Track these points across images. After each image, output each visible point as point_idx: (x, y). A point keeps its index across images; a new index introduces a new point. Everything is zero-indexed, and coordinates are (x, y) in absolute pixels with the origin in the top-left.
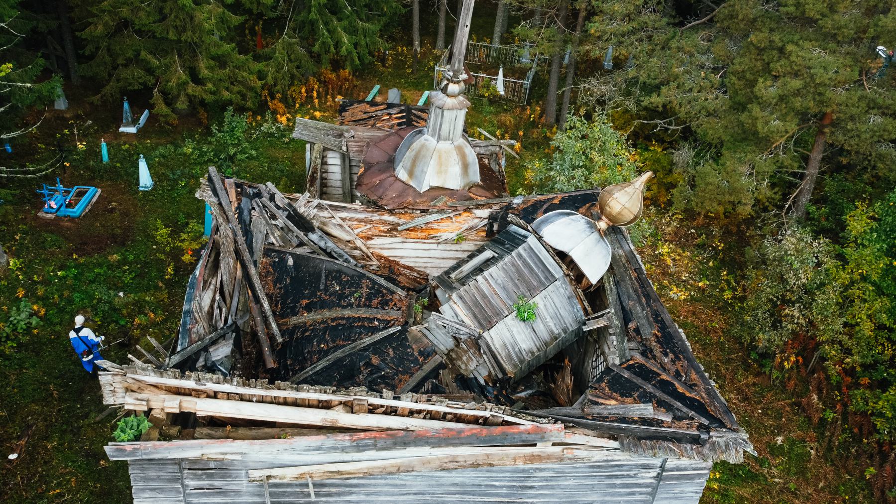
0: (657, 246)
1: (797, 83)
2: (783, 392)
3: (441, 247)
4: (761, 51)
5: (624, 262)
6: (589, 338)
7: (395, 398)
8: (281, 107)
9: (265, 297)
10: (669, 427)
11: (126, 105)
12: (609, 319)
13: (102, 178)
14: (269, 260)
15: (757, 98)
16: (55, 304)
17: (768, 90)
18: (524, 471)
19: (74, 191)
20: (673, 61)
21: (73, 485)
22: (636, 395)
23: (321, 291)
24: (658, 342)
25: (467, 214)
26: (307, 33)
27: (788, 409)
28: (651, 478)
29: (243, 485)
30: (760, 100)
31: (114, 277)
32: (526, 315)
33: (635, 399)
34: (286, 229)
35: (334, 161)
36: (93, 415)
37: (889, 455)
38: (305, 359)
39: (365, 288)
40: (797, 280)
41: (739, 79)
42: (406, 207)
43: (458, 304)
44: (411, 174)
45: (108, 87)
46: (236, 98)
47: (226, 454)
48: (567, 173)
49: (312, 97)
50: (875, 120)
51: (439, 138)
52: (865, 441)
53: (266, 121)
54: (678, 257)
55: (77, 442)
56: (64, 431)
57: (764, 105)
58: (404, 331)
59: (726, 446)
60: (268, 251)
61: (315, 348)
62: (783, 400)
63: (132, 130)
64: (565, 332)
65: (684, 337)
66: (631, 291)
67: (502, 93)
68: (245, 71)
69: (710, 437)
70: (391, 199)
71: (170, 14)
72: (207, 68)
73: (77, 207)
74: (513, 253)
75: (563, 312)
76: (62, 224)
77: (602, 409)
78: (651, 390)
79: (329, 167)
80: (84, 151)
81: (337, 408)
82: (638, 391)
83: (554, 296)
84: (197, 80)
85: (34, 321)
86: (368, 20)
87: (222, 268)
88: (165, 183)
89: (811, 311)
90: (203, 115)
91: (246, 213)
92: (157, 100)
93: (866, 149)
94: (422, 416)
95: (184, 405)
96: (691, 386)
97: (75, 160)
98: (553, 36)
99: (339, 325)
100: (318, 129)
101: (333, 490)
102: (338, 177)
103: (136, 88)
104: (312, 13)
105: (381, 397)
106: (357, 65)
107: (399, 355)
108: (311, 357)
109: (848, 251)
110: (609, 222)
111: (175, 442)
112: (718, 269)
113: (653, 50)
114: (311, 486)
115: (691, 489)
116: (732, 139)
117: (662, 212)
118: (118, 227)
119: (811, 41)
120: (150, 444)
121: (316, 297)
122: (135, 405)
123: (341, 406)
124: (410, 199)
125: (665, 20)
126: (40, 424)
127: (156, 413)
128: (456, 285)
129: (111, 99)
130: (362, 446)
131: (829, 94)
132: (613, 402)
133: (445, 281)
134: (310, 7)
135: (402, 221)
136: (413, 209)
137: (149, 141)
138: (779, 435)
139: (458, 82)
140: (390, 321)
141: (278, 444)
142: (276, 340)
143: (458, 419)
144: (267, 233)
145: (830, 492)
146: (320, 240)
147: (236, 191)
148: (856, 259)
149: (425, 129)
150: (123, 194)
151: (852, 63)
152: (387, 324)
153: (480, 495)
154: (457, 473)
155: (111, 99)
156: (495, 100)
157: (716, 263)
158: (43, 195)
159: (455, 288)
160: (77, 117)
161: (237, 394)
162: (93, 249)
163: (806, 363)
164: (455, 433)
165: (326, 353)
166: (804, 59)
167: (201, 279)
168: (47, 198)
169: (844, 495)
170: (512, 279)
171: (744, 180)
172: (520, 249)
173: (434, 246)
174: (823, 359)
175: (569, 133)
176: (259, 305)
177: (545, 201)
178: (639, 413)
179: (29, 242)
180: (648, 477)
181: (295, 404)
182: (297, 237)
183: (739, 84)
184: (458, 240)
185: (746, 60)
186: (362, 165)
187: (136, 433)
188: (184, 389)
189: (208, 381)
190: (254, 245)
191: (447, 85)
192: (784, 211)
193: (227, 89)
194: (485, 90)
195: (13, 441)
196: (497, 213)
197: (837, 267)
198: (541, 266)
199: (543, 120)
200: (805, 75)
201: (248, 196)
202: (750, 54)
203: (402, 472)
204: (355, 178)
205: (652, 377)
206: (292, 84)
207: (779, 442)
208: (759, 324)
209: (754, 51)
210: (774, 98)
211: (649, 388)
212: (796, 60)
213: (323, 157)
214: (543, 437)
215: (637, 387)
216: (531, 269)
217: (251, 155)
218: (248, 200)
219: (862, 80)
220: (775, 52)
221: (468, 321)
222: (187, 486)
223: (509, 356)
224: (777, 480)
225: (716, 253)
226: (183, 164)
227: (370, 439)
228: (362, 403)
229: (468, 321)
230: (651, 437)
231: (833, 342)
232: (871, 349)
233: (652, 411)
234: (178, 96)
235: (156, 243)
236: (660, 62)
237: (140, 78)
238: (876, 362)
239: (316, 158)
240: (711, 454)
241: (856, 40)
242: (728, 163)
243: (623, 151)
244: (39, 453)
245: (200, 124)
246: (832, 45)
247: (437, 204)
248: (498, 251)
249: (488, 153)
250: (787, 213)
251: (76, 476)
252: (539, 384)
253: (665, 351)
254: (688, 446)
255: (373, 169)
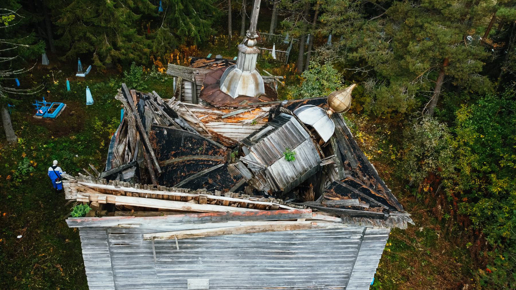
0: (356, 133)
1: (430, 43)
2: (423, 205)
3: (245, 127)
4: (410, 28)
5: (341, 131)
6: (323, 172)
7: (221, 196)
8: (160, 64)
9: (152, 150)
10: (367, 211)
11: (79, 62)
12: (334, 160)
13: (67, 99)
14: (154, 132)
15: (409, 52)
16: (42, 161)
17: (415, 47)
18: (290, 235)
19: (52, 105)
20: (365, 35)
21: (51, 251)
22: (349, 195)
23: (181, 147)
24: (360, 170)
25: (258, 110)
26: (174, 25)
27: (425, 214)
28: (358, 239)
29: (140, 242)
30: (411, 53)
31: (73, 147)
32: (289, 159)
33: (349, 197)
34: (163, 116)
35: (188, 86)
36: (62, 216)
37: (479, 236)
38: (174, 181)
39: (205, 145)
40: (431, 145)
41: (399, 43)
42: (226, 106)
43: (254, 152)
44: (229, 89)
45: (70, 52)
46: (137, 58)
47: (131, 224)
48: (310, 92)
49: (176, 59)
50: (471, 62)
51: (243, 70)
52: (466, 229)
53: (153, 71)
54: (367, 139)
55: (54, 230)
56: (47, 225)
57: (412, 55)
58: (226, 166)
59: (398, 220)
60: (154, 127)
61: (179, 175)
62: (423, 209)
63: (83, 75)
64: (311, 168)
65: (374, 168)
66: (345, 145)
67: (275, 58)
68: (141, 44)
69: (390, 216)
70: (218, 102)
71: (102, 13)
72: (121, 41)
73: (53, 113)
74: (283, 126)
75: (309, 157)
76: (46, 121)
77: (332, 202)
78: (358, 192)
79: (186, 90)
80: (58, 85)
81: (191, 201)
82: (350, 193)
83: (304, 148)
84: (117, 48)
85: (31, 169)
86: (205, 19)
87: (129, 133)
88: (100, 101)
89: (438, 160)
90: (119, 66)
91: (142, 107)
92: (96, 58)
93: (466, 77)
94: (236, 205)
95: (109, 199)
96: (379, 191)
97: (53, 89)
98: (302, 25)
99: (191, 163)
100: (180, 70)
101: (189, 245)
102: (190, 95)
103: (84, 52)
104: (176, 14)
105: (214, 195)
106: (200, 42)
107: (223, 178)
108: (177, 180)
109: (458, 130)
110: (333, 111)
111: (104, 218)
112: (388, 145)
113: (354, 31)
114: (177, 242)
115: (379, 245)
116: (395, 75)
117: (358, 116)
118: (75, 123)
119: (437, 21)
120: (90, 219)
121: (179, 150)
122: (82, 199)
123: (193, 200)
124: (228, 102)
125: (360, 15)
126: (34, 221)
127: (94, 204)
128: (253, 143)
129: (71, 58)
130: (204, 220)
131: (447, 48)
132: (338, 199)
133: (247, 142)
134: (175, 11)
135: (224, 113)
136: (230, 107)
137: (91, 81)
138: (421, 226)
139: (253, 39)
140: (218, 162)
141: (159, 219)
142: (158, 171)
143: (255, 207)
144: (153, 118)
145: (448, 255)
146: (181, 122)
147: (136, 96)
148: (461, 134)
149: (236, 66)
150: (78, 106)
151: (459, 32)
152: (217, 163)
153: (267, 248)
154: (255, 235)
155: (71, 58)
156: (271, 61)
157: (387, 142)
158: (36, 106)
159: (253, 144)
160: (54, 69)
161: (137, 193)
162: (62, 134)
163: (435, 190)
164: (254, 214)
165: (185, 177)
166: (433, 30)
167: (118, 137)
168: (38, 108)
169: (455, 256)
170: (282, 139)
171: (402, 95)
172: (287, 124)
173: (241, 127)
174: (443, 188)
175: (311, 71)
176: (149, 154)
177: (299, 103)
178: (351, 204)
179: (28, 130)
180: (356, 238)
181: (169, 198)
182: (169, 121)
183: (399, 46)
184: (253, 123)
185: (403, 33)
186: (203, 85)
187: (83, 213)
188: (109, 190)
189: (121, 186)
190: (146, 123)
191: (247, 41)
192: (423, 111)
193: (132, 53)
194: (266, 56)
195: (19, 229)
196: (274, 109)
197: (451, 139)
198: (298, 133)
199: (296, 70)
200: (434, 39)
201: (143, 98)
202: (405, 30)
203: (225, 234)
204: (199, 92)
205: (358, 186)
206: (166, 52)
207: (421, 230)
208: (410, 168)
209: (407, 28)
210: (418, 52)
211: (357, 191)
212: (430, 31)
213: (182, 85)
214: (301, 216)
215: (350, 191)
216: (292, 134)
217: (145, 88)
218: (143, 100)
219: (464, 41)
220: (418, 28)
221: (259, 161)
222: (110, 243)
223: (281, 180)
224: (420, 249)
225: (387, 136)
226: (109, 92)
227: (208, 216)
228: (204, 198)
229: (259, 161)
230: (358, 216)
231: (448, 179)
232: (468, 182)
233: (358, 203)
234: (107, 56)
235: (95, 131)
236: (357, 37)
237: (86, 47)
238: (472, 188)
239: (178, 84)
240: (390, 224)
241: (461, 20)
242: (394, 87)
243: (339, 81)
244: (33, 235)
245: (118, 72)
246: (448, 23)
247: (243, 104)
248: (275, 126)
249: (268, 82)
250: (424, 113)
251: (53, 247)
252: (297, 196)
253: (364, 174)
254: (378, 220)
255: (208, 87)
